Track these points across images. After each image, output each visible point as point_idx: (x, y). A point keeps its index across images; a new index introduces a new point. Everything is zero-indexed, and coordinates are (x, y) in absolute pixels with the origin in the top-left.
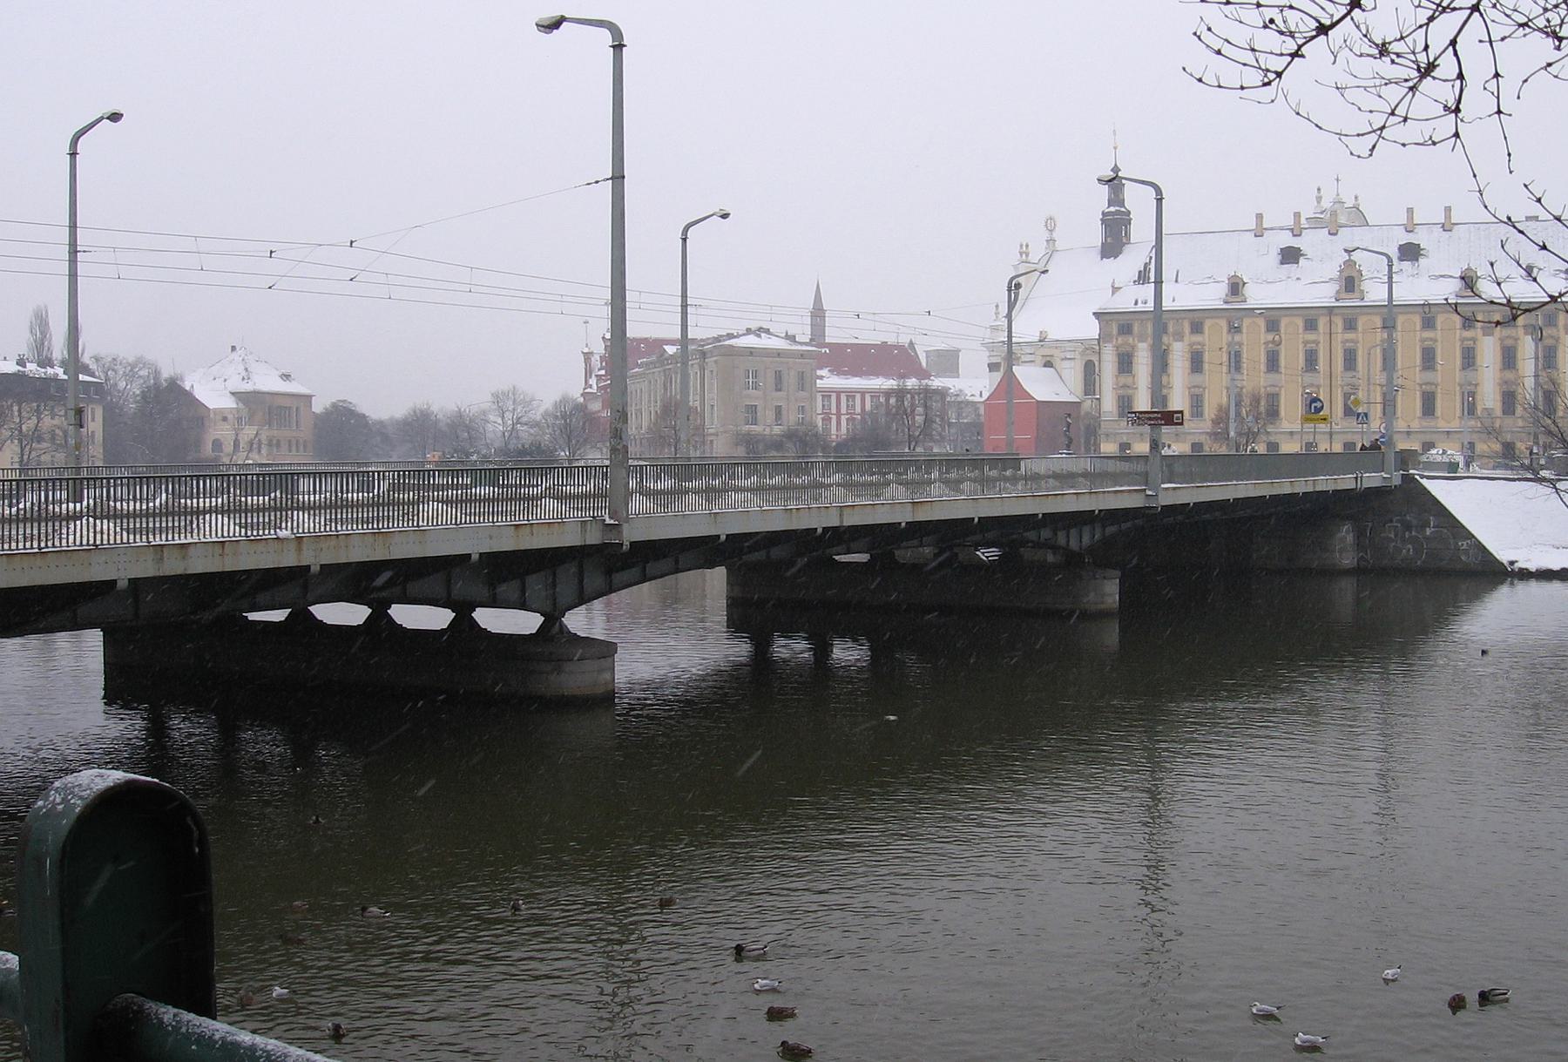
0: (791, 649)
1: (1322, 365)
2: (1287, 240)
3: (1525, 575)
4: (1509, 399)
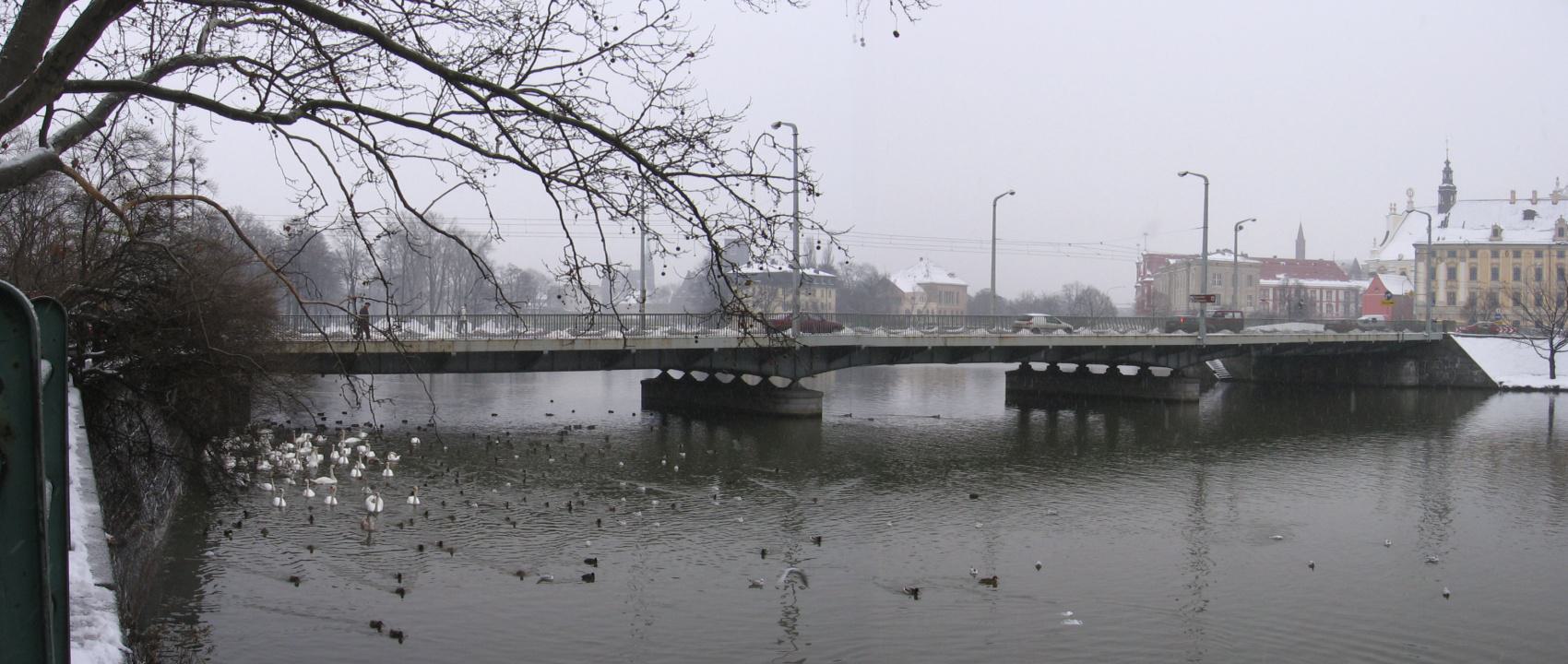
0: (1038, 415)
1: (1545, 276)
2: (1529, 206)
3: (1506, 389)
4: (1452, 298)
